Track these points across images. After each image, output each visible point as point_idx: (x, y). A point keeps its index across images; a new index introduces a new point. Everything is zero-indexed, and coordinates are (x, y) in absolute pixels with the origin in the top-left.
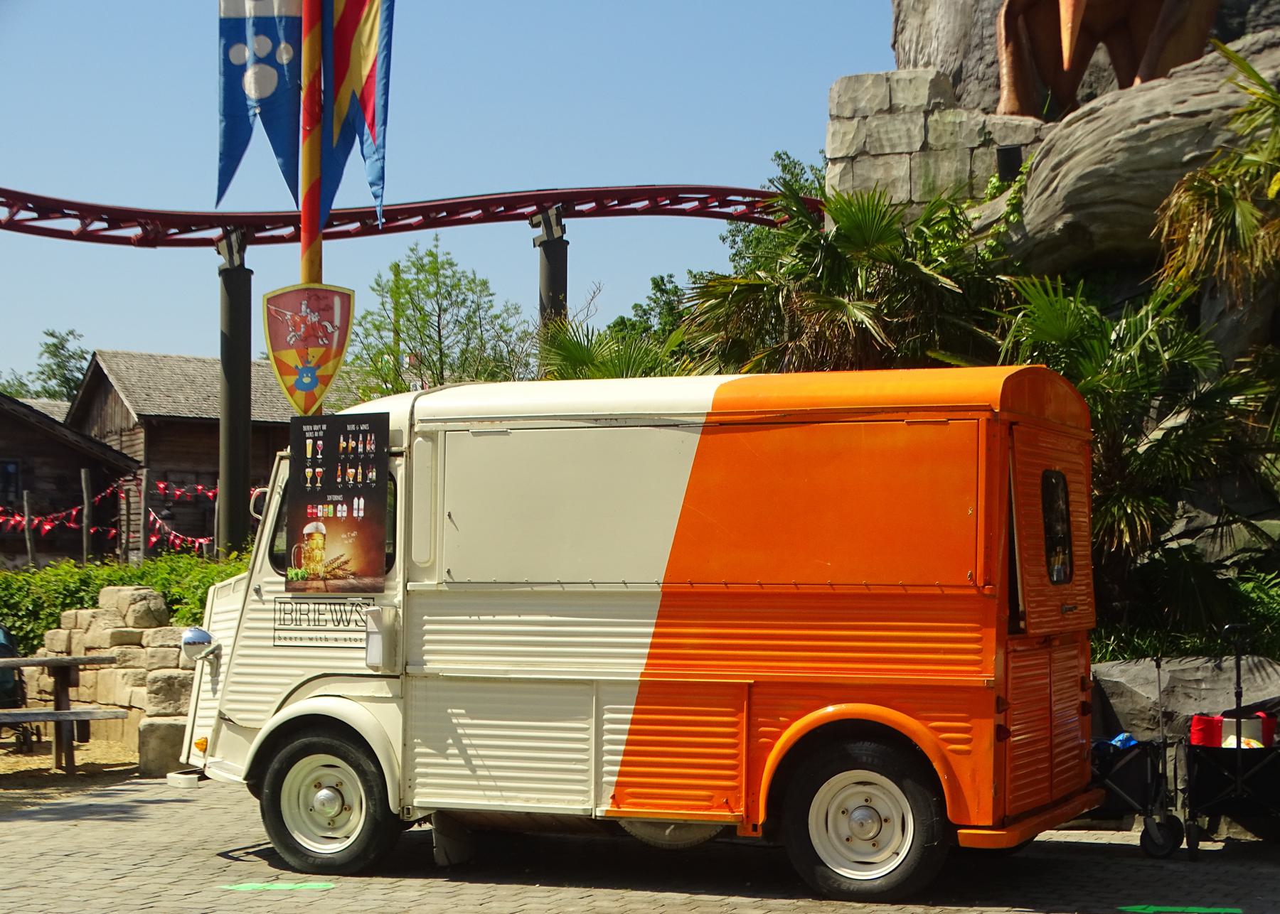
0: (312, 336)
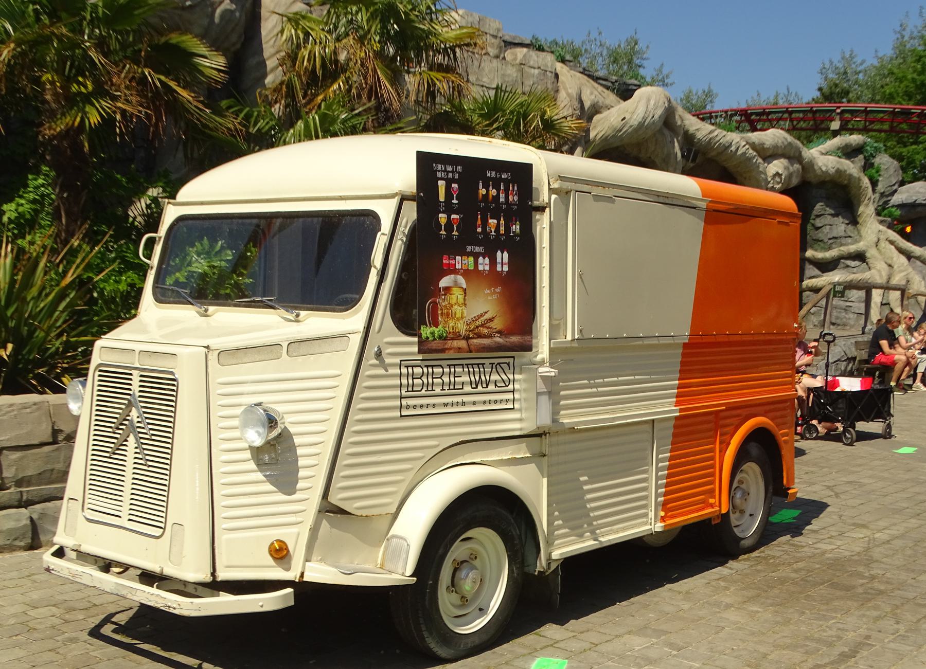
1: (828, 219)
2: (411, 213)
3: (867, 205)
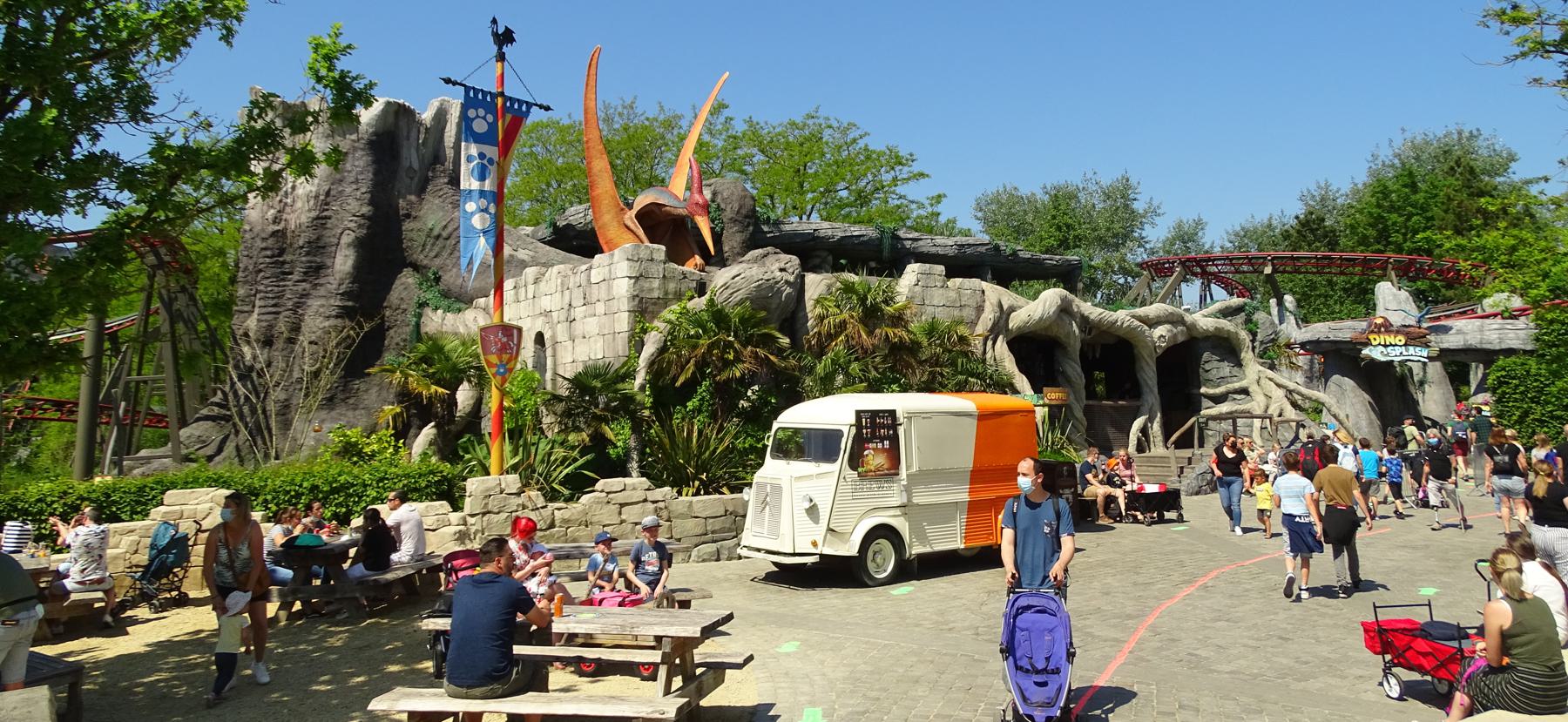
0: (504, 348)
1: (1216, 364)
2: (854, 430)
3: (1247, 352)
